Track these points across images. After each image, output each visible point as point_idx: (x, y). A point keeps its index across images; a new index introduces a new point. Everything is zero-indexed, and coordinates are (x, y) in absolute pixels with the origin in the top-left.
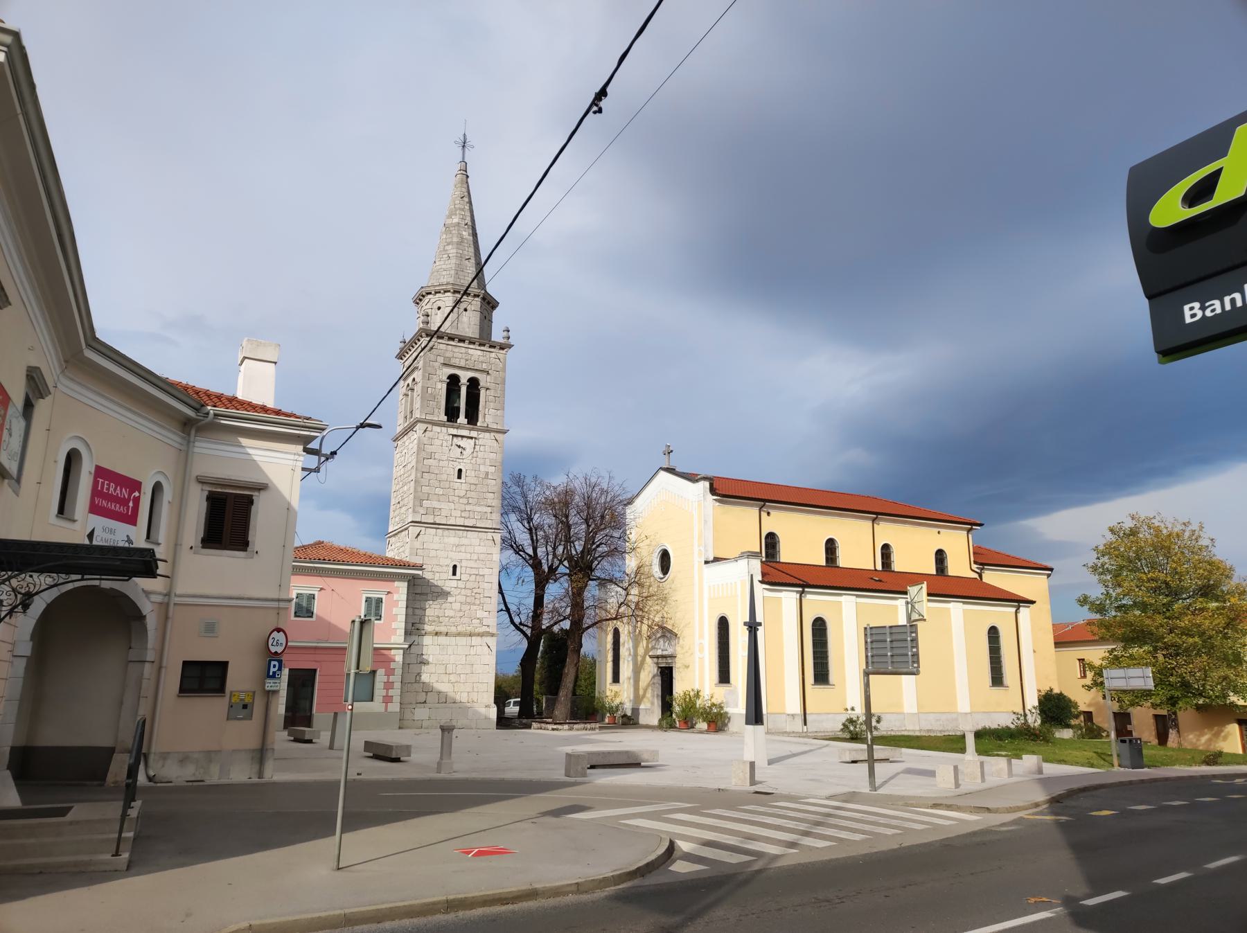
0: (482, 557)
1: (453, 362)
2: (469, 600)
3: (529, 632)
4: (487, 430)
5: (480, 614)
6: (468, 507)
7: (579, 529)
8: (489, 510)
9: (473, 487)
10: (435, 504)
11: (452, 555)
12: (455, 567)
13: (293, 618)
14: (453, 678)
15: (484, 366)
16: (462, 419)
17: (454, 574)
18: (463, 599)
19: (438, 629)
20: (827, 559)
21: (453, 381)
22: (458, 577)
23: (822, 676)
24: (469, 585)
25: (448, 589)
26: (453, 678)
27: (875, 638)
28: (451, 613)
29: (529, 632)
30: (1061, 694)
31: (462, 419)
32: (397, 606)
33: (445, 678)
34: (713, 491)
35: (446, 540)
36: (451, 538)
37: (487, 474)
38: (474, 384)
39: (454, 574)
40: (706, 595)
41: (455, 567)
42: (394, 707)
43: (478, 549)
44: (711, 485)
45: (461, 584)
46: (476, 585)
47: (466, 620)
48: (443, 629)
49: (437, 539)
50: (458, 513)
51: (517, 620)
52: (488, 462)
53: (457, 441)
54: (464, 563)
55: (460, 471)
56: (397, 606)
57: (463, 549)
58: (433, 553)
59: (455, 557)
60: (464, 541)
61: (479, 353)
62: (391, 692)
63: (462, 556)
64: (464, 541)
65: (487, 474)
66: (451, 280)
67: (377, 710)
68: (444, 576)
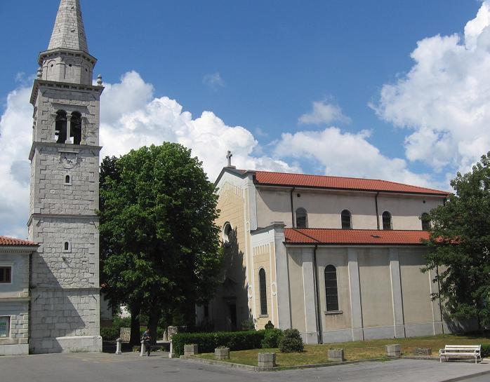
5: (87, 275)
9: (77, 188)
10: (50, 201)
12: (66, 244)
16: (69, 113)
17: (66, 248)
20: (343, 224)
22: (69, 250)
23: (332, 304)
25: (84, 319)
28: (66, 275)
31: (69, 113)
34: (256, 182)
37: (87, 178)
39: (66, 248)
40: (252, 255)
41: (66, 244)
44: (254, 178)
55: (68, 177)
59: (66, 237)
61: (81, 94)
63: (72, 235)
65: (87, 178)
66: (60, 46)
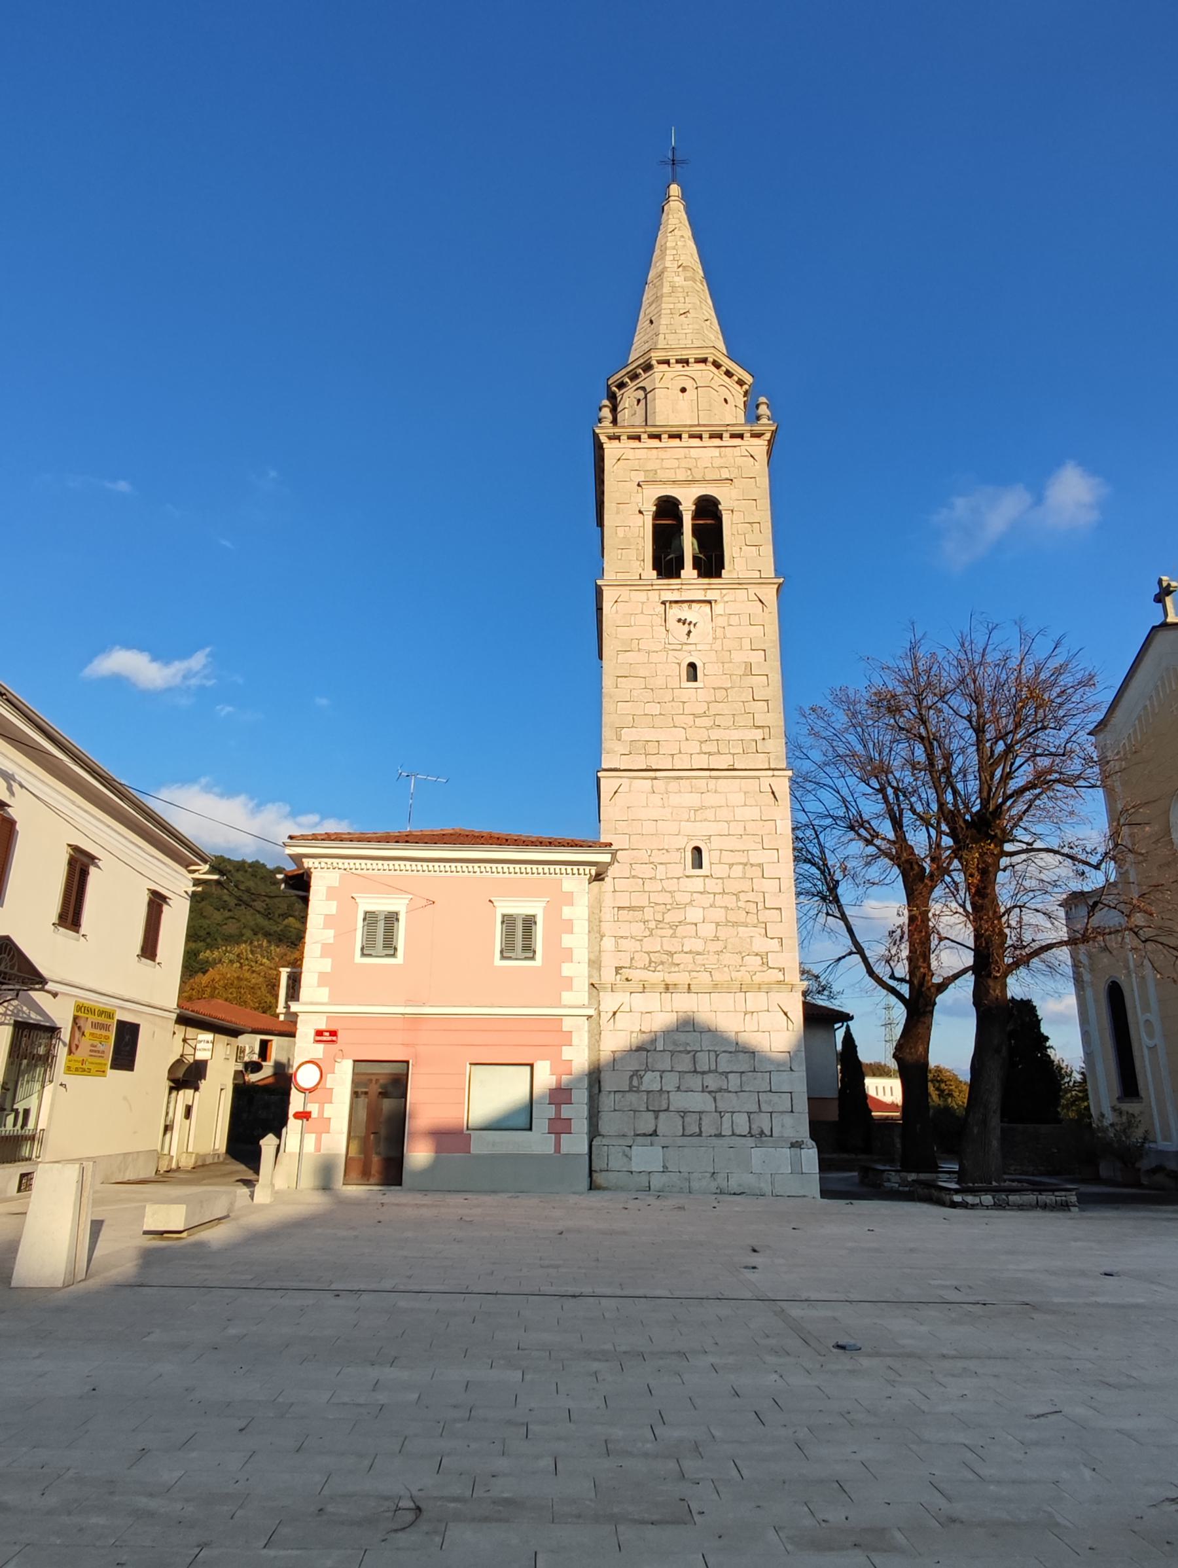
0: (751, 827)
1: (662, 475)
2: (732, 917)
3: (905, 989)
4: (740, 584)
5: (760, 944)
6: (715, 734)
7: (966, 760)
8: (758, 734)
9: (721, 694)
11: (687, 827)
13: (358, 959)
14: (712, 1082)
15: (725, 474)
18: (719, 914)
19: (670, 979)
21: (667, 508)
24: (733, 886)
26: (712, 1082)
27: (104, 1033)
28: (698, 945)
29: (905, 989)
30: (935, 1004)
32: (330, 889)
33: (695, 1082)
35: (675, 799)
36: (684, 796)
38: (708, 508)
42: (576, 1143)
43: (741, 813)
45: (712, 885)
46: (746, 885)
47: (728, 958)
48: (682, 978)
49: (655, 799)
50: (694, 747)
51: (882, 970)
52: (746, 644)
53: (675, 612)
54: (716, 843)
56: (330, 889)
57: (709, 814)
58: (649, 827)
59: (696, 833)
60: (710, 800)
62: (566, 1111)
64: (710, 800)
67: (538, 1149)
68: (677, 870)
